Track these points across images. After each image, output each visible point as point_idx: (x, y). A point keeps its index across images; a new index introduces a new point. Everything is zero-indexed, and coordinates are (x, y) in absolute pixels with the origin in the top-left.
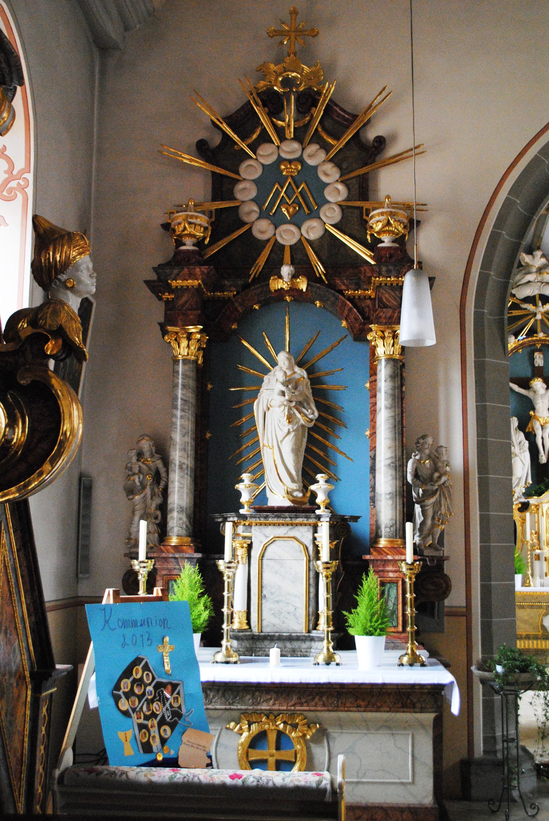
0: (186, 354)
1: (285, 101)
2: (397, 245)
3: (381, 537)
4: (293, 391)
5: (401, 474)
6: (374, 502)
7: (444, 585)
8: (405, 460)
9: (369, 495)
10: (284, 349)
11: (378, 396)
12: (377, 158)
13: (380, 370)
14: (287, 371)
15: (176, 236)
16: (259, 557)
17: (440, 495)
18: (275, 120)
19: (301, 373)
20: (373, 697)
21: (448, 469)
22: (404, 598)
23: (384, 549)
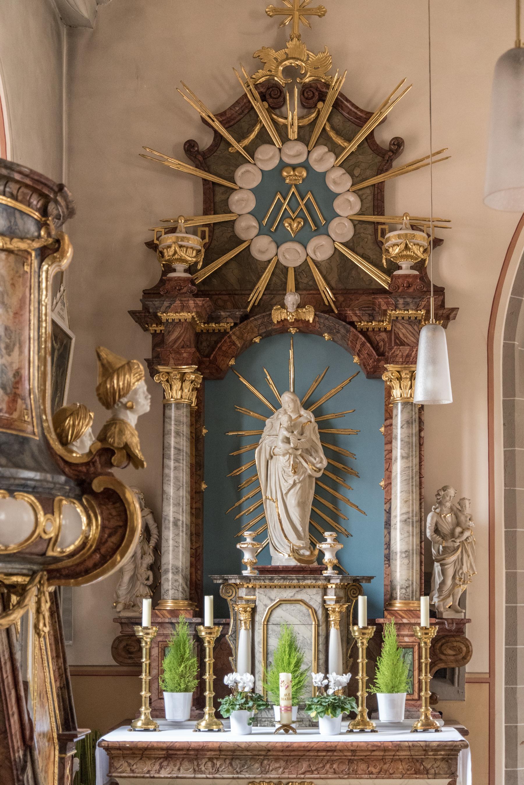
0: (179, 397)
1: (288, 94)
2: (416, 273)
3: (396, 599)
4: (299, 437)
5: (418, 530)
6: (389, 560)
7: (464, 649)
8: (423, 514)
9: (383, 552)
10: (288, 390)
11: (393, 444)
12: (394, 163)
13: (396, 415)
14: (292, 415)
15: (166, 261)
16: (264, 622)
17: (462, 552)
18: (275, 117)
19: (307, 415)
20: (385, 764)
21: (471, 523)
22: (420, 664)
23: (399, 612)
